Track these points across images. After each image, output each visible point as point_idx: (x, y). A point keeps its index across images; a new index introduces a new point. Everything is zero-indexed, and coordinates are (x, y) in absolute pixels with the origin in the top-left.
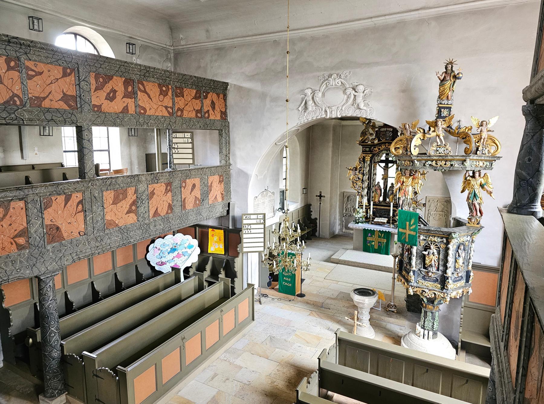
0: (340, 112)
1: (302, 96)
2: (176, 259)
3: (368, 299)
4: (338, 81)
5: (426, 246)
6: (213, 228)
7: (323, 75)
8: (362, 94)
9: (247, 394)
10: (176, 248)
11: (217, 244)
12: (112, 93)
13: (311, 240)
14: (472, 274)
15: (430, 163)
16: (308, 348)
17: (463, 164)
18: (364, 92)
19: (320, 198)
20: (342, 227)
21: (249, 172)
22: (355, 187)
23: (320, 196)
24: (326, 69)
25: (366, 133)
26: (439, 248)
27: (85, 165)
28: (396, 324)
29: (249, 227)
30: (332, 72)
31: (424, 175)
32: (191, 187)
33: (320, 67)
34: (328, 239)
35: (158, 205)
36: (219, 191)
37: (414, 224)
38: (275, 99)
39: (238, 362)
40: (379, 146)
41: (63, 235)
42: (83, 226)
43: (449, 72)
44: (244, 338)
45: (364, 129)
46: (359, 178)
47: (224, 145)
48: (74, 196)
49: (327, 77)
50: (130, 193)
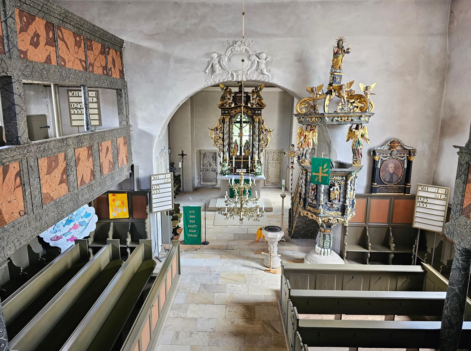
0: (245, 76)
1: (208, 59)
2: (72, 230)
3: (279, 234)
4: (243, 47)
5: (332, 184)
6: (114, 192)
7: (228, 41)
8: (264, 61)
9: (219, 340)
10: (72, 219)
11: (119, 208)
12: (36, 38)
13: (178, 195)
14: (355, 201)
15: (336, 118)
16: (240, 286)
17: (359, 119)
18: (266, 60)
19: (183, 157)
20: (200, 181)
21: (153, 133)
22: (217, 145)
23: (183, 155)
24: (230, 35)
25: (225, 98)
26: (340, 184)
27: (18, 127)
28: (289, 250)
29: (158, 188)
30: (236, 39)
31: (270, 132)
32: (105, 151)
33: (224, 34)
34: (191, 192)
35: (84, 172)
36: (124, 154)
37: (327, 168)
38: (180, 61)
39: (189, 315)
40: (235, 109)
41: (4, 218)
42: (23, 204)
43: (341, 47)
44: (179, 292)
45: (224, 94)
46: (220, 137)
47: (124, 105)
48: (11, 166)
49: (232, 44)
50: (61, 159)
